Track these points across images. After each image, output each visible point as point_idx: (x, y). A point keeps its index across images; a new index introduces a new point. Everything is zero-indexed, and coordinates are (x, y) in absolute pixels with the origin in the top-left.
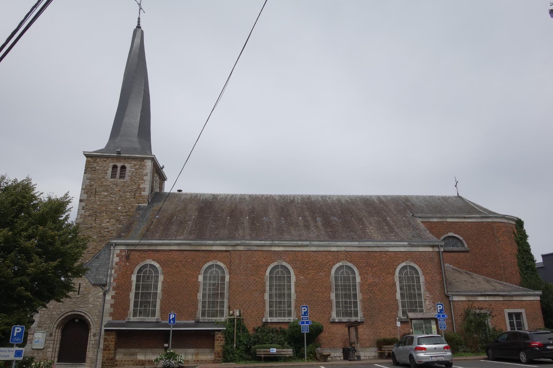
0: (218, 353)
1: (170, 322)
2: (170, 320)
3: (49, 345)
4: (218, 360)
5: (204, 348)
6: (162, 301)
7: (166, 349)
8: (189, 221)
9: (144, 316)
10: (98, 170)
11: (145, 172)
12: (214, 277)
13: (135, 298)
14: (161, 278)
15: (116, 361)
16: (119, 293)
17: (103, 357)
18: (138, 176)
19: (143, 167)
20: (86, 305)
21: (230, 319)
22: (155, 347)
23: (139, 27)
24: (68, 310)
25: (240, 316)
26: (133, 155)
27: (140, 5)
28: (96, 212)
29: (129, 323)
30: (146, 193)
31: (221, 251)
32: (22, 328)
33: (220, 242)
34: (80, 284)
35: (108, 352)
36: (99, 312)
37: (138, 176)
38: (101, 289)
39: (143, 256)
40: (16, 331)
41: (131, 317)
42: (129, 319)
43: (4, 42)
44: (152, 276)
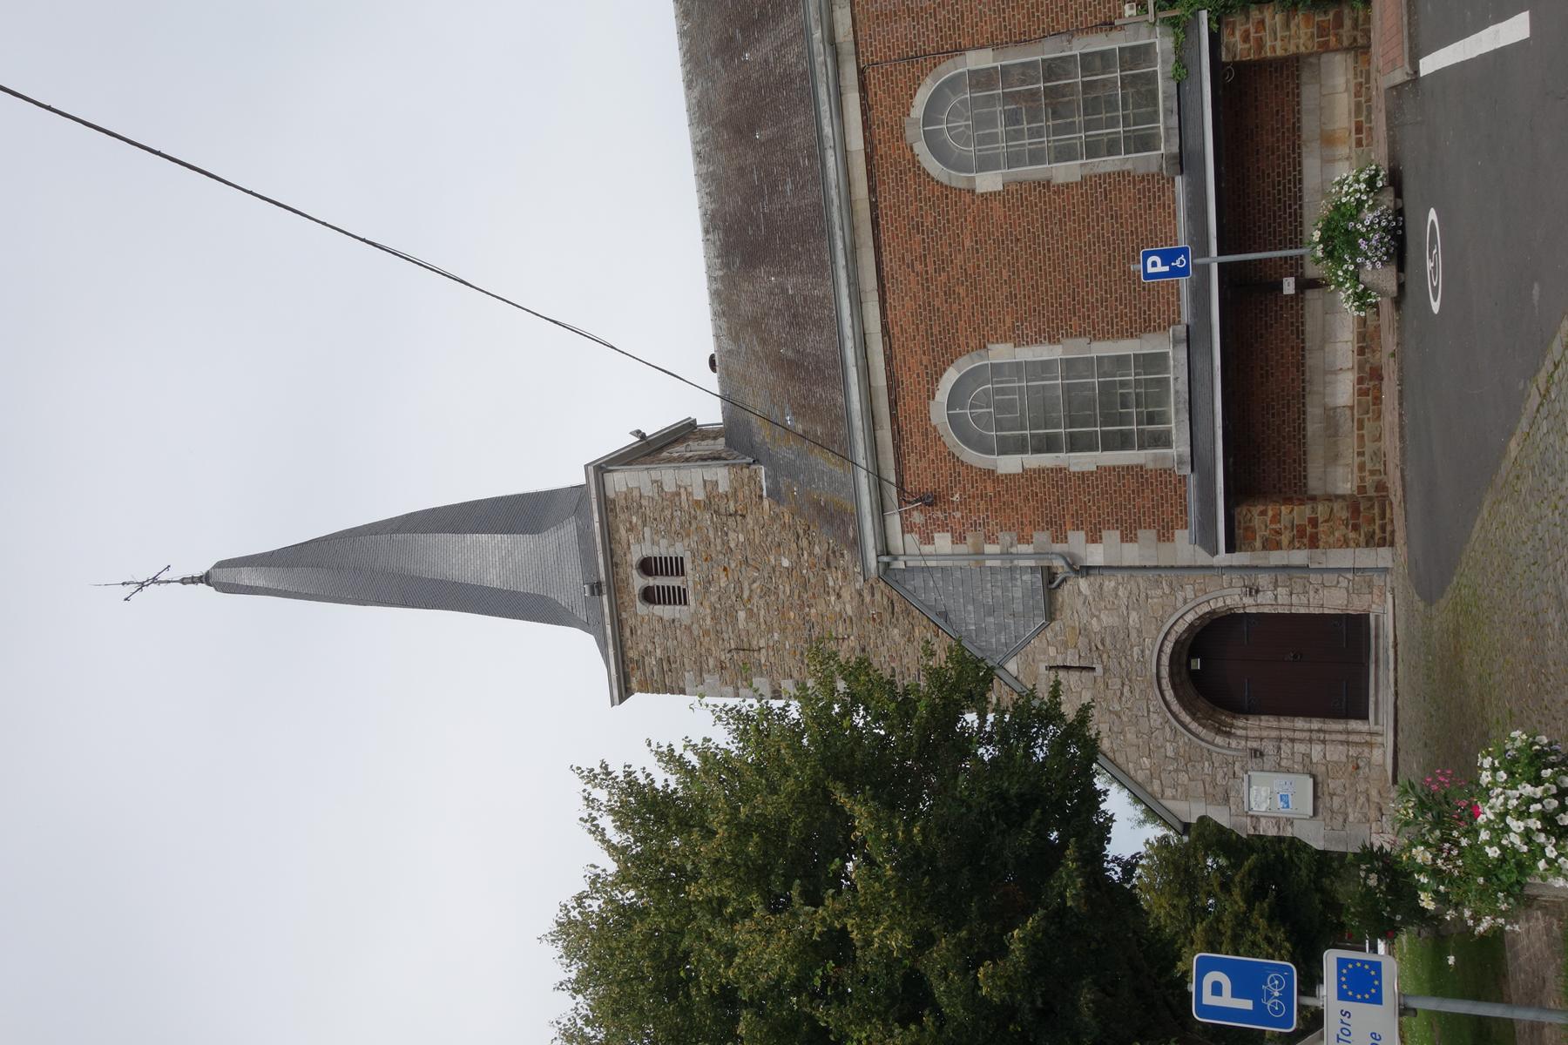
0: (1322, 31)
1: (1183, 272)
2: (1175, 272)
3: (1298, 758)
4: (1355, 26)
5: (1297, 112)
6: (1097, 334)
7: (1305, 285)
8: (784, 291)
9: (1167, 403)
10: (666, 649)
11: (648, 490)
12: (980, 122)
15: (1362, 489)
17: (1345, 543)
18: (667, 513)
19: (633, 502)
20: (1134, 634)
22: (1300, 333)
23: (205, 579)
26: (598, 540)
27: (142, 585)
29: (1196, 458)
30: (721, 476)
31: (865, 110)
32: (1205, 967)
33: (826, 122)
35: (1322, 528)
36: (1158, 583)
37: (667, 513)
38: (1066, 587)
39: (917, 438)
40: (1227, 1000)
41: (1172, 452)
42: (1181, 462)
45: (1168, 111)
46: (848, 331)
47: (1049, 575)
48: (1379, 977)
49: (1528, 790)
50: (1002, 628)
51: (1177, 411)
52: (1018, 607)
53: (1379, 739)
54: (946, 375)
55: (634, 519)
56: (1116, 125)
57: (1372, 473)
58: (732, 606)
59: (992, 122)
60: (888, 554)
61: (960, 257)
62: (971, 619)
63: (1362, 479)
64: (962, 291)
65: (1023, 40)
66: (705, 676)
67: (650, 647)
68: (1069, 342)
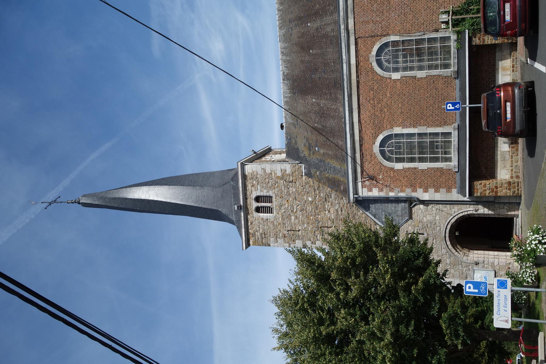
1: (458, 109)
3: (490, 264)
8: (319, 104)
11: (260, 172)
14: (398, 130)
15: (512, 177)
16: (420, 183)
18: (267, 180)
19: (254, 176)
20: (437, 223)
21: (453, 26)
24: (444, 246)
25: (447, 12)
26: (241, 189)
27: (50, 204)
28: (317, 227)
35: (499, 189)
37: (267, 180)
39: (368, 157)
40: (472, 290)
42: (455, 167)
43: (61, 323)
44: (396, 143)
45: (454, 58)
46: (347, 122)
48: (506, 283)
49: (536, 236)
51: (454, 151)
52: (399, 213)
55: (254, 182)
56: (438, 61)
57: (515, 172)
58: (289, 214)
59: (397, 58)
60: (357, 195)
61: (386, 99)
63: (512, 174)
65: (409, 33)
66: (278, 239)
67: (258, 229)
68: (420, 127)
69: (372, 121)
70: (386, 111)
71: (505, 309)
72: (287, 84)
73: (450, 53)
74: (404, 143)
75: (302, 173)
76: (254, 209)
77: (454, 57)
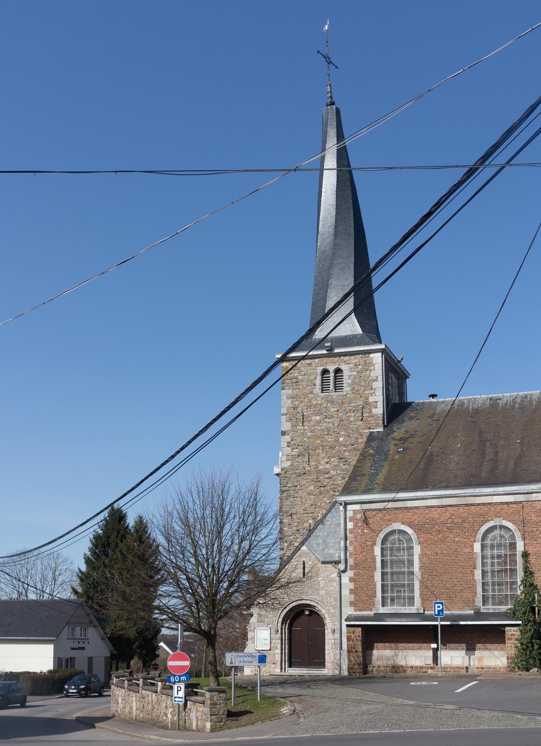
3: (276, 645)
11: (373, 374)
13: (383, 580)
14: (417, 550)
18: (363, 383)
19: (368, 366)
28: (307, 449)
30: (379, 410)
31: (507, 503)
34: (304, 562)
36: (335, 600)
37: (363, 383)
38: (334, 569)
39: (388, 517)
47: (337, 563)
50: (318, 544)
53: (283, 671)
54: (410, 529)
55: (360, 367)
61: (452, 536)
62: (322, 534)
64: (440, 536)
66: (290, 400)
68: (420, 573)
69: (428, 521)
70: (439, 536)
71: (242, 662)
72: (484, 404)
73: (499, 605)
74: (403, 556)
75: (373, 429)
76: (328, 367)
77: (495, 609)
